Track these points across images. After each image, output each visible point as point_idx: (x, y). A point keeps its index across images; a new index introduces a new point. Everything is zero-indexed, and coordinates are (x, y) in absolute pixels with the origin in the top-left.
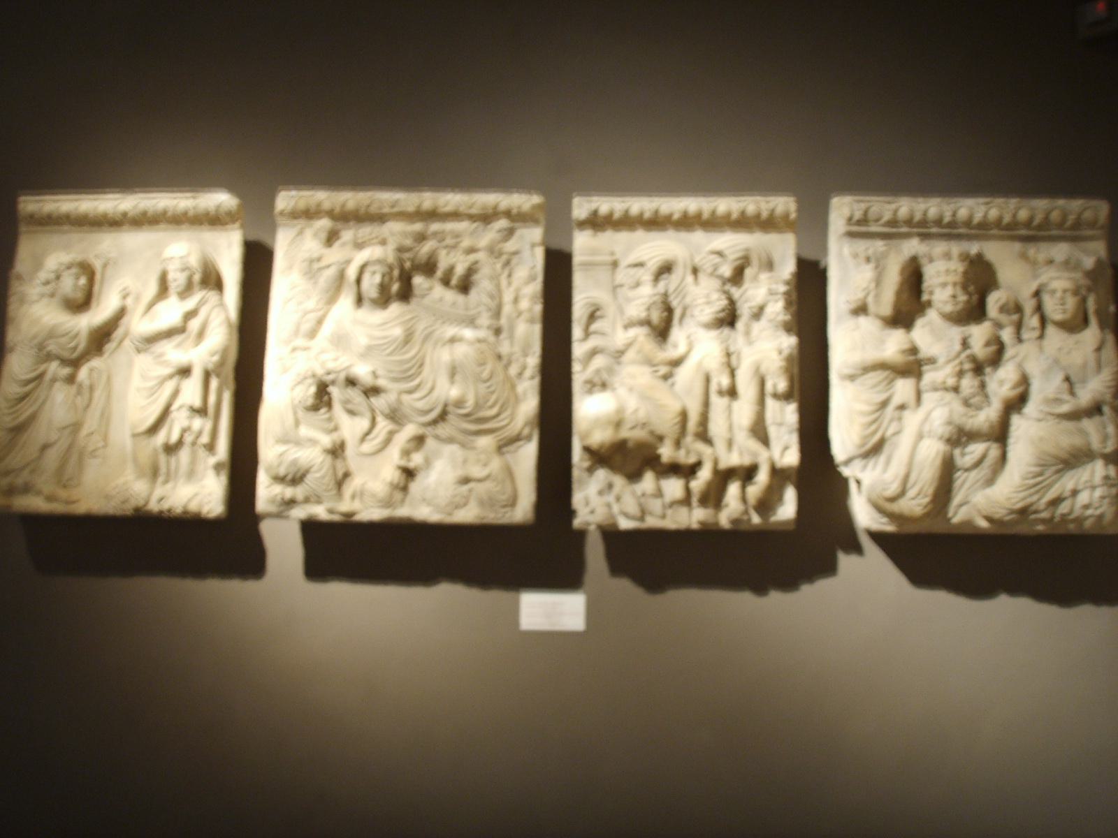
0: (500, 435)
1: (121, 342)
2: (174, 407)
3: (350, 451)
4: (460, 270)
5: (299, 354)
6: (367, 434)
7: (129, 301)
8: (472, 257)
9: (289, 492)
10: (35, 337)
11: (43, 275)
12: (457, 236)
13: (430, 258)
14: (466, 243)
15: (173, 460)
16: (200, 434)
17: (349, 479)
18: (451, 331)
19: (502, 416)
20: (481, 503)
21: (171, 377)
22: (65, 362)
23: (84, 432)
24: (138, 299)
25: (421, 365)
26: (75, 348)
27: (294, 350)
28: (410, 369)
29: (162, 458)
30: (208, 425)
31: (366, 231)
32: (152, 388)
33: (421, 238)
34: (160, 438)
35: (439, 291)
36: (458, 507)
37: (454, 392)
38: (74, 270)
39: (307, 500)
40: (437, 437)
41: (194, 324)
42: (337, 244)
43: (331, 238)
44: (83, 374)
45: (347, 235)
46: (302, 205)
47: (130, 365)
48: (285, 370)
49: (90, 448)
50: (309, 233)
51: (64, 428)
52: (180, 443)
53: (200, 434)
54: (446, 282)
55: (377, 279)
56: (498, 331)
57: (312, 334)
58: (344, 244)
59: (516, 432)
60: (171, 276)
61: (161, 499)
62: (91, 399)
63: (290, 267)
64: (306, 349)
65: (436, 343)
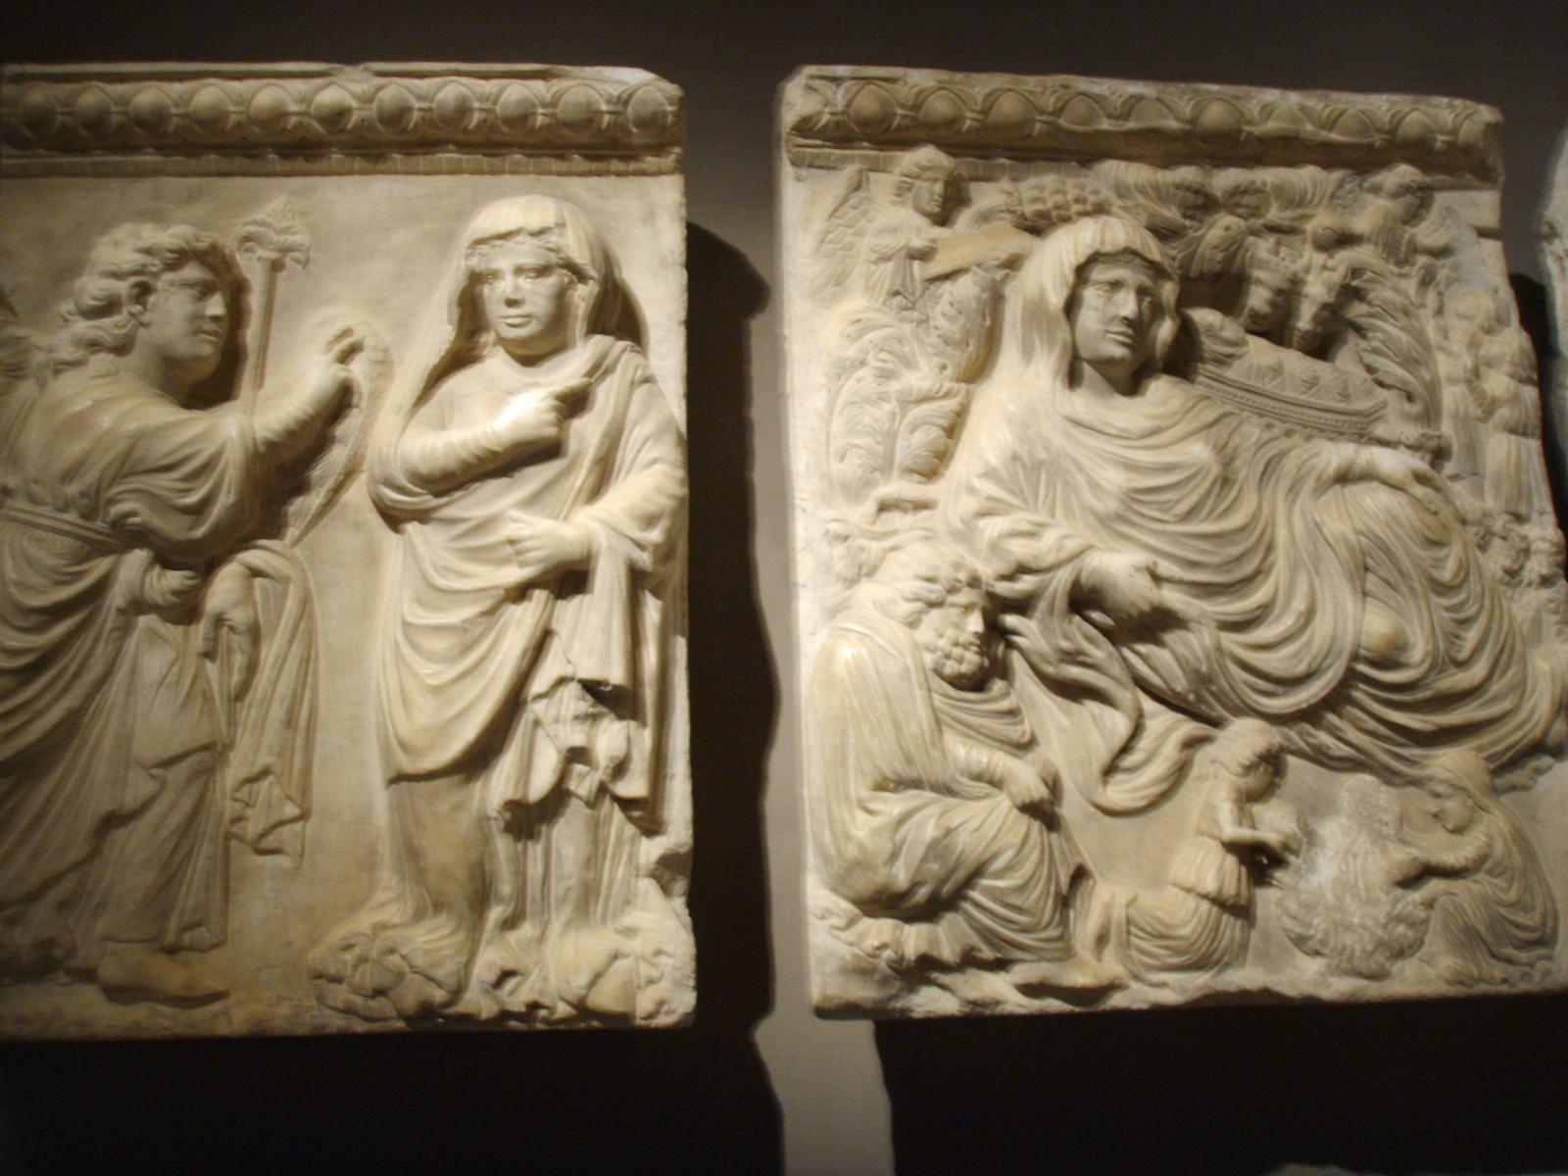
0: (1493, 744)
1: (338, 489)
2: (540, 683)
3: (1071, 808)
4: (1317, 290)
5: (895, 519)
6: (1125, 749)
7: (358, 369)
8: (1345, 257)
9: (914, 939)
10: (70, 475)
11: (93, 286)
12: (1295, 200)
13: (1230, 258)
14: (1321, 221)
15: (536, 850)
16: (620, 769)
17: (1085, 887)
18: (1335, 454)
19: (1495, 688)
20: (1468, 938)
21: (520, 593)
22: (166, 556)
23: (236, 769)
24: (384, 365)
25: (1270, 548)
26: (199, 510)
27: (883, 507)
28: (1239, 559)
29: (503, 845)
30: (646, 738)
31: (1043, 187)
32: (462, 629)
33: (1203, 204)
34: (499, 785)
35: (1260, 352)
36: (1400, 953)
37: (1375, 625)
38: (192, 272)
39: (969, 961)
40: (1320, 757)
41: (586, 432)
42: (964, 218)
43: (947, 208)
44: (224, 589)
45: (987, 196)
46: (867, 103)
47: (372, 559)
48: (864, 571)
49: (253, 827)
50: (882, 185)
51: (169, 762)
52: (558, 797)
53: (620, 769)
54: (1274, 328)
55: (1127, 305)
56: (1439, 455)
57: (934, 465)
58: (985, 217)
59: (1537, 733)
60: (494, 294)
61: (506, 975)
62: (252, 668)
63: (839, 281)
64: (921, 506)
65: (1294, 489)
